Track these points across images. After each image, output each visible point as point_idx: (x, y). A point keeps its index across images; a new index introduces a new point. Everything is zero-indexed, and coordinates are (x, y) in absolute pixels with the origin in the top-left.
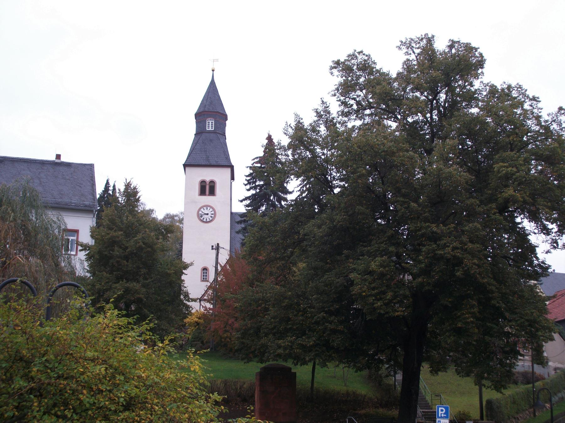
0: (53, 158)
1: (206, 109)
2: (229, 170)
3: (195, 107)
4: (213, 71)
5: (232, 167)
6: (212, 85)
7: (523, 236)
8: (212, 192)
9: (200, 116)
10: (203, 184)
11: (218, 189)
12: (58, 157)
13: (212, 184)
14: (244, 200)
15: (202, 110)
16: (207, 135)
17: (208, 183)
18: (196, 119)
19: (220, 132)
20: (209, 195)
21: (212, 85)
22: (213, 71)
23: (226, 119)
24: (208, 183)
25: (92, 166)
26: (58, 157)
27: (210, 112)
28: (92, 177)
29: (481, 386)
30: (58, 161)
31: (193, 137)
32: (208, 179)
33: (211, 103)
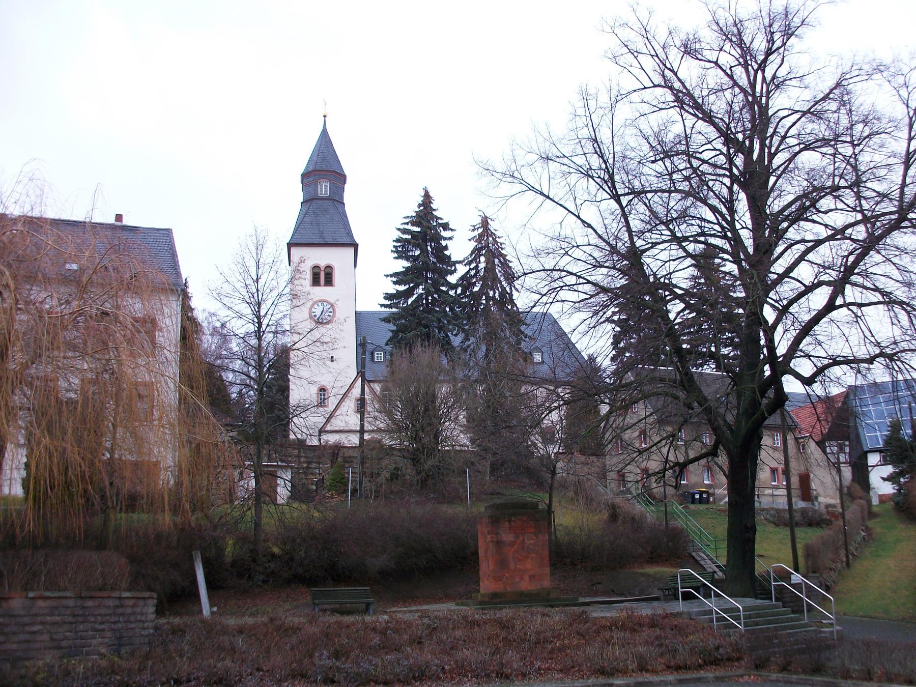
0: (111, 220)
1: (318, 168)
2: (352, 250)
3: (300, 164)
4: (325, 116)
5: (355, 246)
6: (325, 135)
7: (642, 574)
8: (329, 281)
9: (309, 177)
10: (316, 270)
11: (337, 277)
12: (119, 217)
13: (328, 270)
14: (391, 276)
15: (311, 169)
16: (320, 202)
17: (323, 269)
18: (302, 182)
19: (336, 200)
20: (325, 286)
21: (325, 135)
22: (325, 116)
23: (345, 183)
24: (323, 269)
25: (168, 233)
26: (119, 217)
27: (323, 171)
28: (171, 245)
29: (854, 356)
30: (119, 223)
31: (299, 207)
32: (323, 264)
33: (324, 159)
